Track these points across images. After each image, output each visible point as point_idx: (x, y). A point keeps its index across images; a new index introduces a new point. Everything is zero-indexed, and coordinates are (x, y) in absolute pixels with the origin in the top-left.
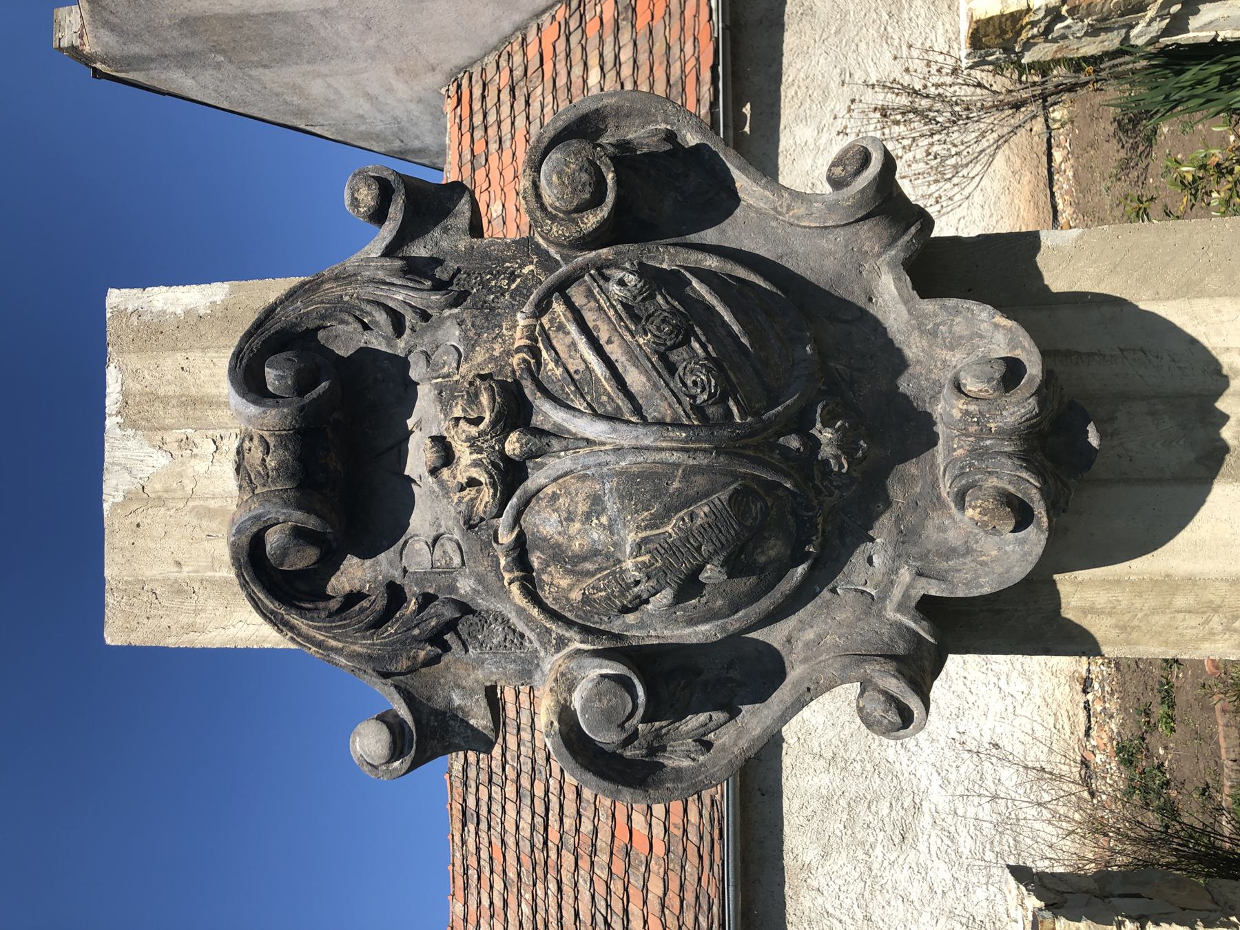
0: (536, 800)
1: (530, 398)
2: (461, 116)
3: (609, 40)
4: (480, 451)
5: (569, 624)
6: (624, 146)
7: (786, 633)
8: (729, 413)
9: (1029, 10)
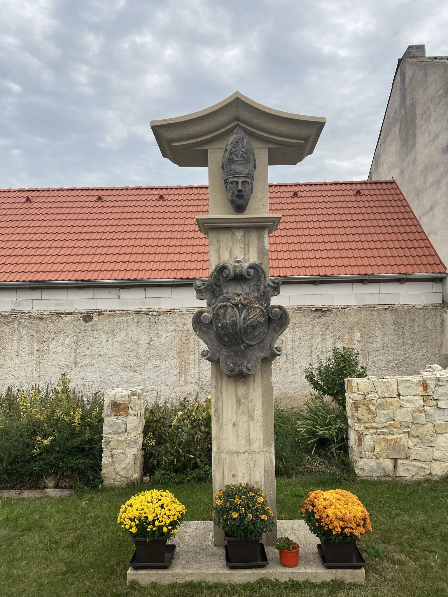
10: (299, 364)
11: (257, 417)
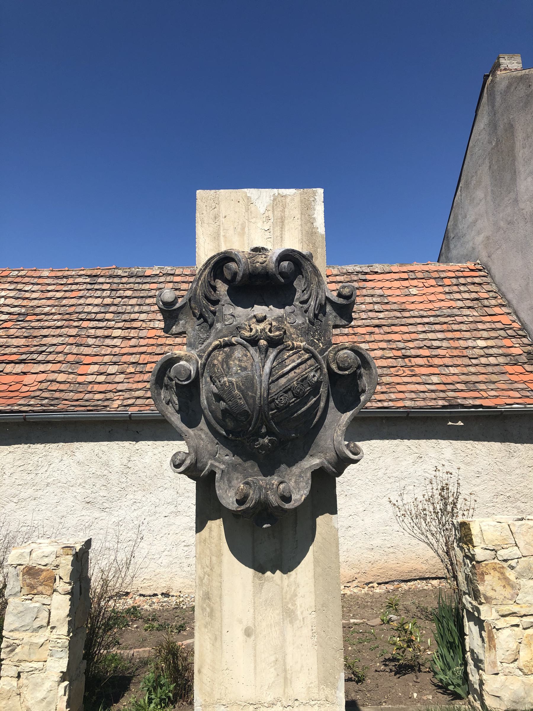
0: (103, 315)
1: (277, 348)
2: (465, 271)
3: (500, 351)
4: (261, 332)
5: (207, 359)
6: (361, 376)
7: (204, 429)
8: (272, 410)
9: (474, 547)
10: (359, 498)
11: (302, 613)
